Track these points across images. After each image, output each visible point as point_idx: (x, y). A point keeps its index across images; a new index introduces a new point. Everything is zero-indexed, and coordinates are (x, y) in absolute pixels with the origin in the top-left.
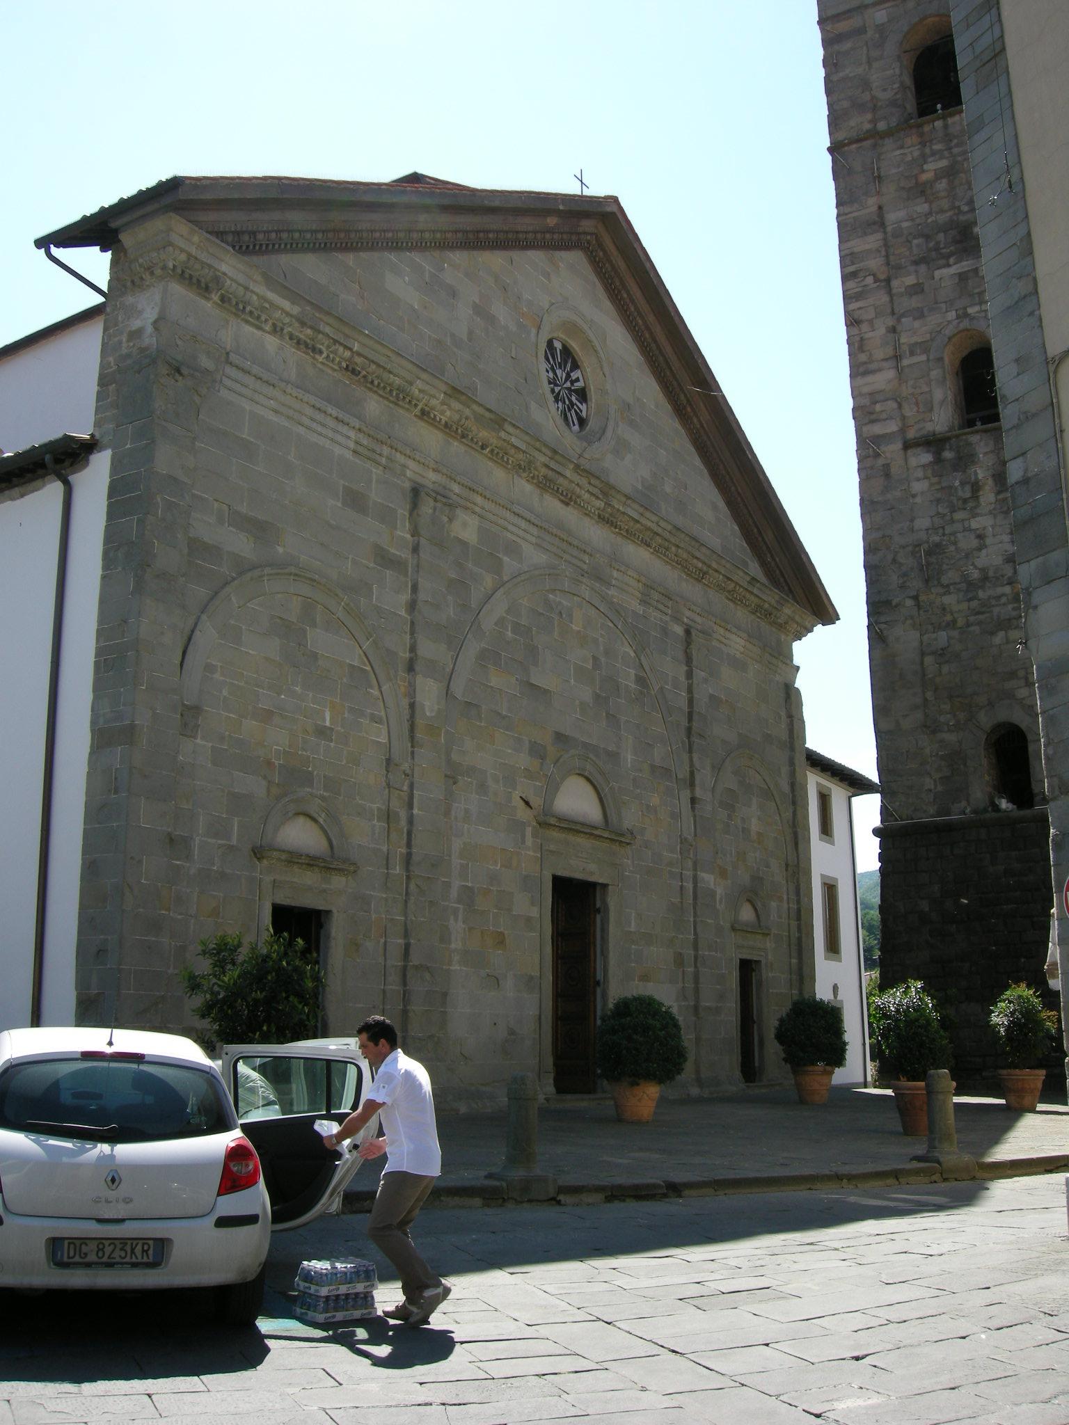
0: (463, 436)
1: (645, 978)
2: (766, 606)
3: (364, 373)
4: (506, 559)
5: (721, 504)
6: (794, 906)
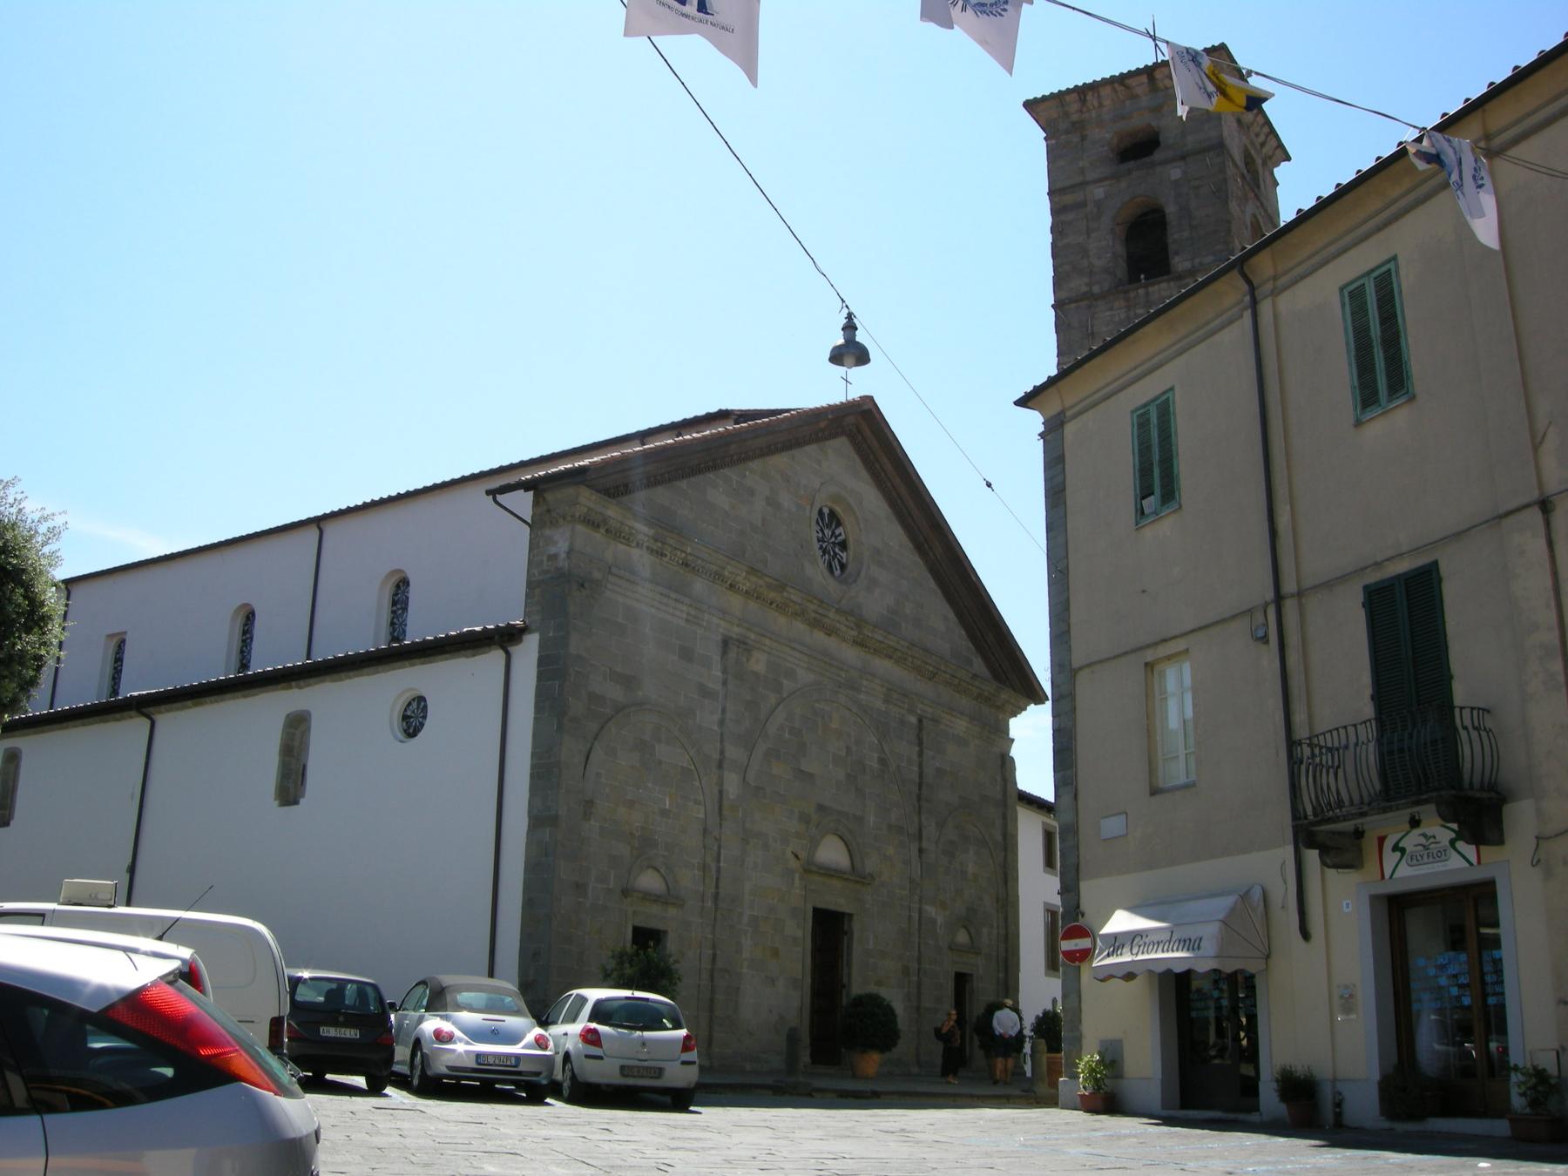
0: (757, 598)
1: (879, 983)
2: (986, 694)
3: (693, 565)
4: (785, 682)
5: (951, 615)
6: (1003, 932)
